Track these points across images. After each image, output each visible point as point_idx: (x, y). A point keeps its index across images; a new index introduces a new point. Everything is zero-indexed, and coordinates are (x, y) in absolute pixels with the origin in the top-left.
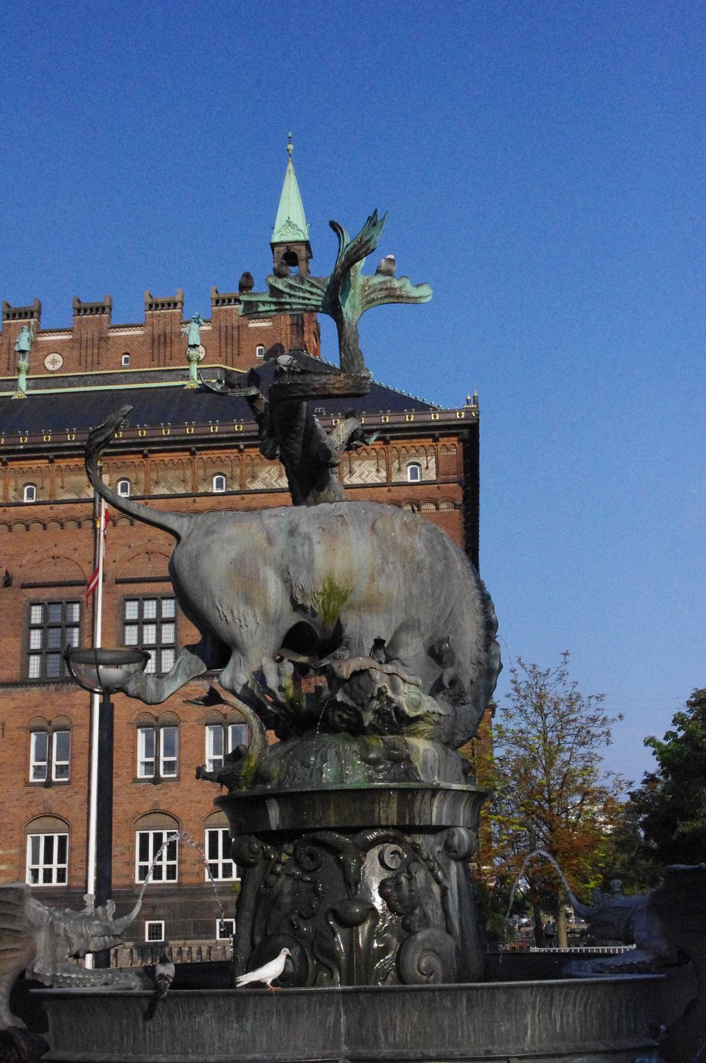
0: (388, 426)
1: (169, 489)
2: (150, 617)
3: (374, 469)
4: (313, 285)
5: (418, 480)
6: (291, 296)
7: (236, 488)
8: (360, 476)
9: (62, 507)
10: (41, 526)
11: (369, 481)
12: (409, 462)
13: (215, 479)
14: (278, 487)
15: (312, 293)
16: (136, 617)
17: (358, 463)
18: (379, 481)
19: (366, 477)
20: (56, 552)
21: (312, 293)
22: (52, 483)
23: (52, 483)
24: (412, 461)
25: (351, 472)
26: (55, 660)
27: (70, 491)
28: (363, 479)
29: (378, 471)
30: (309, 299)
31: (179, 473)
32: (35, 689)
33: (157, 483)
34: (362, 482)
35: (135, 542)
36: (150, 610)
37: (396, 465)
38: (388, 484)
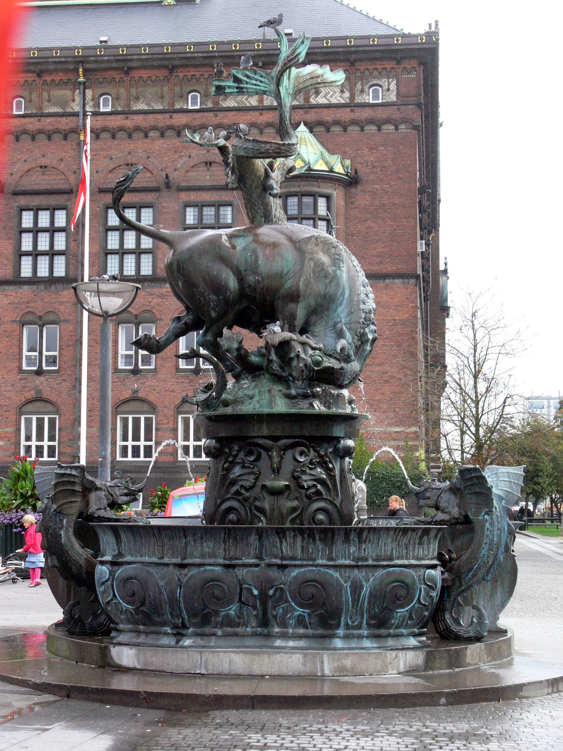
1: (147, 104)
5: (380, 101)
6: (247, 83)
7: (210, 105)
8: (325, 96)
9: (49, 120)
11: (334, 101)
12: (371, 83)
14: (248, 105)
15: (261, 82)
18: (343, 101)
19: (331, 97)
20: (43, 161)
21: (261, 82)
22: (40, 96)
23: (40, 96)
24: (374, 82)
26: (130, 260)
27: (54, 105)
28: (328, 100)
31: (157, 89)
32: (26, 287)
33: (137, 98)
34: (327, 102)
35: (115, 153)
36: (44, 220)
37: (359, 86)
38: (352, 105)
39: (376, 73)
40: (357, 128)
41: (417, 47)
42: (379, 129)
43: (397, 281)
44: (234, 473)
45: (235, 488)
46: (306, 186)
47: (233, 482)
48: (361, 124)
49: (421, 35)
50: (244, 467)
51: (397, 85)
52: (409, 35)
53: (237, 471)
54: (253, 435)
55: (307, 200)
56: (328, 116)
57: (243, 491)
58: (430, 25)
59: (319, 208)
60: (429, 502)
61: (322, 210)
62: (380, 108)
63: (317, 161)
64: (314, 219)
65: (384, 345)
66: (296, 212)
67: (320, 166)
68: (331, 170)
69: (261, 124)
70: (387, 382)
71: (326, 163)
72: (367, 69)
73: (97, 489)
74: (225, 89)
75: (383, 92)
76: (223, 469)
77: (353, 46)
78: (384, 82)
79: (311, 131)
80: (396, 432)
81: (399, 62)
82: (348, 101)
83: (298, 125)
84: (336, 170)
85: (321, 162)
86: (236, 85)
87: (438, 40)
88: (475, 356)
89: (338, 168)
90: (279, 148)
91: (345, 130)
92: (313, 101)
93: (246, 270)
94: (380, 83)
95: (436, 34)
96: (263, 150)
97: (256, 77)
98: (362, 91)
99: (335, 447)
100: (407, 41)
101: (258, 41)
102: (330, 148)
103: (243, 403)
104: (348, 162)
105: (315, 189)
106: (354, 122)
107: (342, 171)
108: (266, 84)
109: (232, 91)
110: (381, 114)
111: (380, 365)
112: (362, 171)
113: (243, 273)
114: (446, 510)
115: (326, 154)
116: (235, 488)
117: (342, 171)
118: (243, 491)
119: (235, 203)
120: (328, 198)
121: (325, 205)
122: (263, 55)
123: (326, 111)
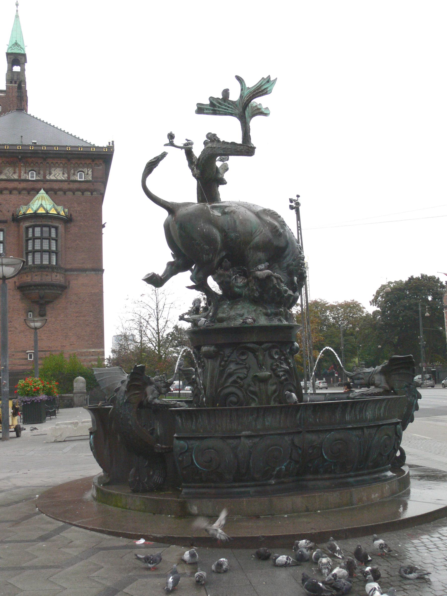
0: (70, 152)
2: (46, 241)
3: (61, 173)
4: (229, 104)
5: (83, 180)
6: (219, 107)
8: (54, 176)
10: (63, 193)
12: (79, 170)
13: (78, 174)
14: (13, 178)
15: (229, 107)
16: (36, 241)
17: (53, 169)
18: (64, 179)
19: (57, 176)
21: (229, 107)
24: (80, 170)
25: (50, 174)
28: (56, 177)
29: (63, 174)
30: (228, 110)
34: (55, 179)
37: (72, 171)
38: (69, 181)
39: (81, 165)
40: (71, 193)
41: (103, 153)
42: (83, 194)
43: (93, 272)
44: (231, 369)
45: (231, 380)
46: (45, 221)
47: (230, 375)
48: (73, 191)
49: (105, 148)
50: (237, 364)
51: (92, 172)
52: (98, 147)
53: (233, 367)
54: (246, 341)
55: (46, 229)
56: (56, 186)
57: (239, 381)
58: (109, 143)
59: (52, 233)
60: (362, 381)
61: (53, 235)
62: (83, 183)
63: (51, 209)
64: (49, 239)
65: (86, 306)
66: (39, 235)
67: (53, 212)
68: (59, 214)
69: (19, 189)
70: (87, 325)
71: (56, 210)
72: (76, 163)
73: (151, 383)
74: (204, 110)
75: (83, 175)
76: (220, 365)
77: (70, 151)
78: (86, 170)
79: (47, 193)
80: (93, 352)
81: (93, 161)
82: (66, 179)
83: (40, 190)
84: (61, 214)
85: (53, 209)
86: (212, 108)
87: (113, 150)
88: (157, 310)
89: (62, 213)
90: (248, 149)
91: (65, 194)
92: (48, 178)
93: (228, 229)
94: (83, 170)
95: (113, 147)
96: (238, 150)
97: (225, 104)
98: (74, 174)
99: (291, 348)
100: (98, 150)
101: (19, 145)
102: (57, 202)
103: (235, 320)
104: (66, 210)
105: (50, 223)
106: (70, 190)
107: (64, 214)
108: (232, 109)
109: (209, 112)
110: (84, 186)
111: (84, 316)
112: (74, 214)
113: (227, 231)
114: (380, 386)
115: (56, 206)
116: (231, 380)
117: (64, 214)
118: (239, 381)
119: (5, 230)
120: (56, 228)
121: (55, 232)
122: (22, 153)
123: (55, 183)
